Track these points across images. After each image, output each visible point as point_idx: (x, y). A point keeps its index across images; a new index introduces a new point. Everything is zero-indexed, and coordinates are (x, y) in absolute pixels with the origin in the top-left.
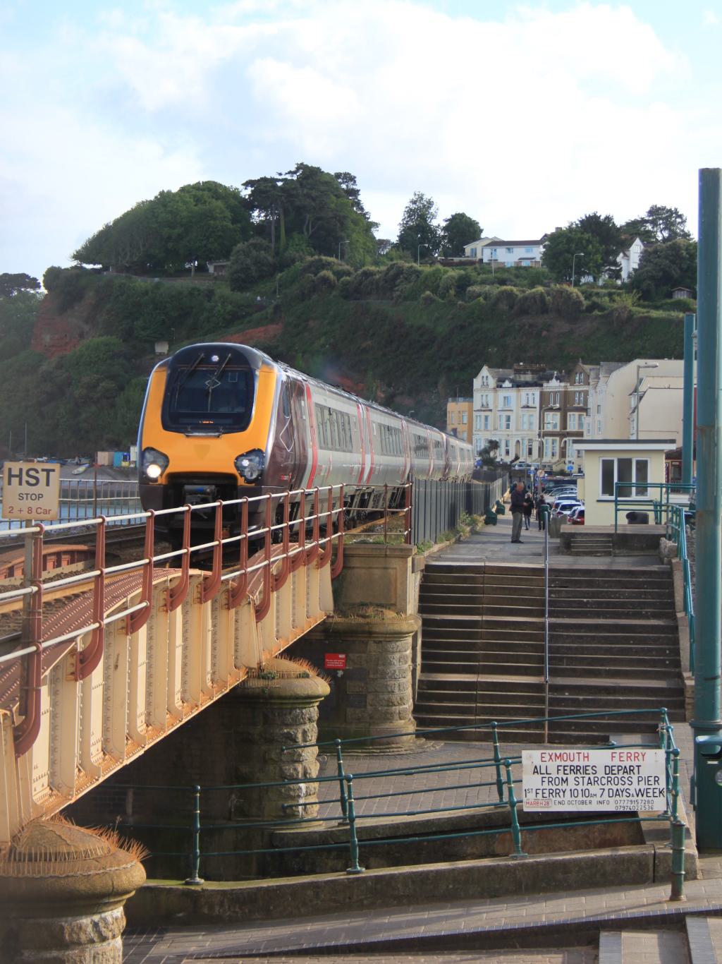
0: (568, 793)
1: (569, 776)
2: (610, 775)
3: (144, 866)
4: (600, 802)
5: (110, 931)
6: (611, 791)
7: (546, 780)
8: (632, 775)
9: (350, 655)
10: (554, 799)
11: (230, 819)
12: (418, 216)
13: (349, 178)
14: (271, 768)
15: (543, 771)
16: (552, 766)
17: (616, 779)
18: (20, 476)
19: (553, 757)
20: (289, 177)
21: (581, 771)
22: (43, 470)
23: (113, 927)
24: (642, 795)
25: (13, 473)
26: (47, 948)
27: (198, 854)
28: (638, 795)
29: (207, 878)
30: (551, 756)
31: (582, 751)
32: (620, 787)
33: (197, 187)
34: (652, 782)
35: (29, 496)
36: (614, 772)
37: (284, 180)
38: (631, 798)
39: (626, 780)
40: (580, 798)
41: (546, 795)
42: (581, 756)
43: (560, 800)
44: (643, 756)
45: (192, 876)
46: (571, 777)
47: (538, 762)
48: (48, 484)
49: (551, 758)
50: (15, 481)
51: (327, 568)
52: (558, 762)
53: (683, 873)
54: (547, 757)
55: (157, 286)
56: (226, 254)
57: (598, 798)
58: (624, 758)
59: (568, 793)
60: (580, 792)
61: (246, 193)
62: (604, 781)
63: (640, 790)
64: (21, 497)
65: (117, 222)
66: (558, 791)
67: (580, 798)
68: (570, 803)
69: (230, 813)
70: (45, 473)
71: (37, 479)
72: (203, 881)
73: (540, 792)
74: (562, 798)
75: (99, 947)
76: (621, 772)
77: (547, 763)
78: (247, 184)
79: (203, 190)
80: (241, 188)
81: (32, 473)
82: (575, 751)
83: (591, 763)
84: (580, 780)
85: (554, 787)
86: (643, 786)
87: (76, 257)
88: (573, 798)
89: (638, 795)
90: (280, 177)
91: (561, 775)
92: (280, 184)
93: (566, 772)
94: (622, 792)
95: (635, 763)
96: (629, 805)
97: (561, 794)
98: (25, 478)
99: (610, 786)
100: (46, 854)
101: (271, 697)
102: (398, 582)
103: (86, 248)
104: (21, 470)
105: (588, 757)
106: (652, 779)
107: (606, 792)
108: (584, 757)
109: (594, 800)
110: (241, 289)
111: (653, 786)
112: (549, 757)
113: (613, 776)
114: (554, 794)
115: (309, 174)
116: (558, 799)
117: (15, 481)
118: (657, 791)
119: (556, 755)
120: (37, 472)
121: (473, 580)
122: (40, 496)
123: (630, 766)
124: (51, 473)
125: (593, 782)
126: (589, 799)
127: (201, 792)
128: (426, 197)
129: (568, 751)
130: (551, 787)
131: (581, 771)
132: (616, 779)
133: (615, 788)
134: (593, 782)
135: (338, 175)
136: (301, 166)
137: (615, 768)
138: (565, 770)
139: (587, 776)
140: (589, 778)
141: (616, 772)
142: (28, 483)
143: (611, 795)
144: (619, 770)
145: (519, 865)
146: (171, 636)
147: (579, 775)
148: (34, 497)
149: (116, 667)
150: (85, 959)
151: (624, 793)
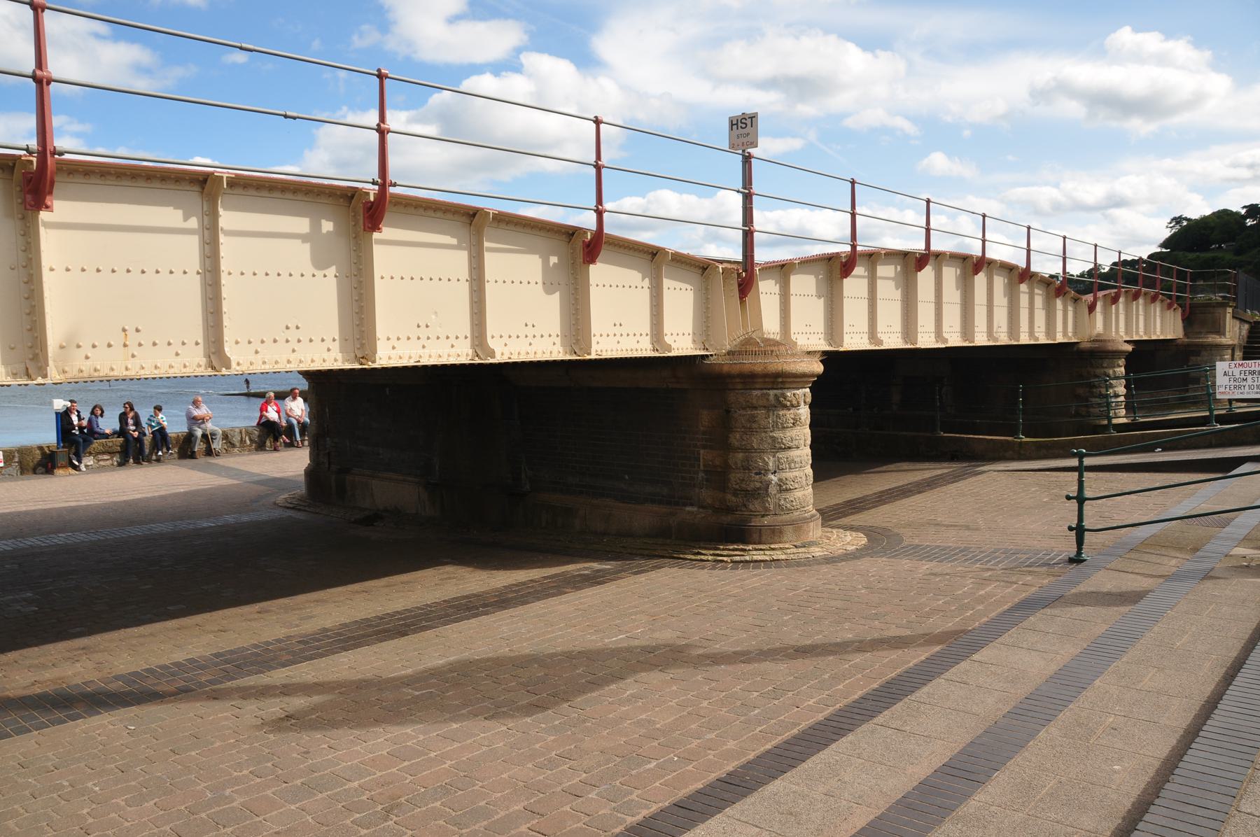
0: (1247, 387)
1: (1248, 377)
16: (1237, 371)
18: (737, 124)
19: (1237, 366)
22: (749, 118)
25: (733, 123)
41: (1232, 388)
46: (1250, 377)
47: (1227, 369)
50: (735, 127)
52: (1241, 368)
54: (1233, 366)
55: (1198, 257)
59: (1247, 387)
60: (1255, 386)
61: (1243, 212)
67: (1255, 390)
68: (1248, 393)
71: (746, 124)
82: (1253, 361)
85: (1238, 384)
91: (1242, 376)
97: (1242, 387)
98: (740, 124)
103: (1164, 242)
104: (737, 120)
116: (1240, 391)
117: (735, 127)
120: (746, 120)
122: (748, 134)
129: (1247, 362)
130: (1235, 383)
142: (741, 127)
146: (1176, 395)
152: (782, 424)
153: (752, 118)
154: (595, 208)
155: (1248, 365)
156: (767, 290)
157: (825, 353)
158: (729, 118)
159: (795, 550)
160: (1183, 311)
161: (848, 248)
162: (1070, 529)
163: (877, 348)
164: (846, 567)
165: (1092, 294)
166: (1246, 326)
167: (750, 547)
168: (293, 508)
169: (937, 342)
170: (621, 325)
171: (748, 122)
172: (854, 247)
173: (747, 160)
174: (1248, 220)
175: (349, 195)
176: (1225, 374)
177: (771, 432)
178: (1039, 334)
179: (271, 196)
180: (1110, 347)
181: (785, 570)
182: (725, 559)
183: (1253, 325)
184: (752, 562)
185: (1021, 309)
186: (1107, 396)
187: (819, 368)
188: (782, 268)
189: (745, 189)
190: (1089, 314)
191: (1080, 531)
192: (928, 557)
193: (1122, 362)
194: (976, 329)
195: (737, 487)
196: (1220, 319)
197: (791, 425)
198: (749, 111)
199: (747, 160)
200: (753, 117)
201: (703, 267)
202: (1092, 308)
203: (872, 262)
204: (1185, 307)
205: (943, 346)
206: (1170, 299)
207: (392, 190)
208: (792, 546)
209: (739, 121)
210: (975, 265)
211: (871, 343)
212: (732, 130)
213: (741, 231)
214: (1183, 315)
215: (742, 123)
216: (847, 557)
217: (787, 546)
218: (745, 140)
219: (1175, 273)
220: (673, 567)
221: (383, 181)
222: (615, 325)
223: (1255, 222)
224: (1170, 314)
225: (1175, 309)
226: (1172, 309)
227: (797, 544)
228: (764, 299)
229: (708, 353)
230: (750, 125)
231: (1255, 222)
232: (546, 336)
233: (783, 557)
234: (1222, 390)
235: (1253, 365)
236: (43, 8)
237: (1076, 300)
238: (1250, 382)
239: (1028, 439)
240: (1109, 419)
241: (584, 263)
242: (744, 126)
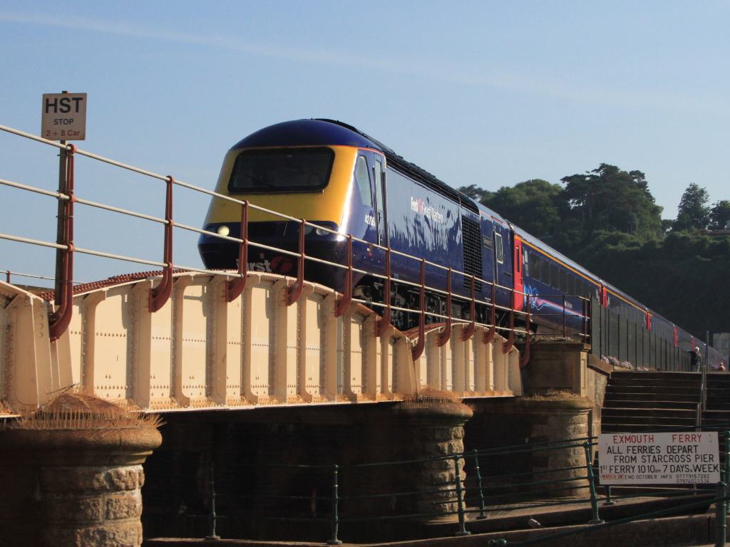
0: (636, 469)
2: (672, 454)
3: (161, 433)
4: (664, 477)
5: (123, 482)
6: (673, 467)
7: (618, 458)
8: (690, 453)
10: (626, 474)
12: (693, 197)
13: (639, 174)
15: (616, 451)
16: (623, 447)
17: (677, 457)
18: (55, 105)
19: (624, 439)
20: (594, 174)
21: (648, 450)
22: (74, 99)
23: (126, 479)
24: (700, 471)
25: (53, 108)
27: (337, 520)
28: (695, 471)
30: (622, 438)
31: (648, 434)
32: (680, 463)
33: (528, 183)
34: (707, 459)
35: (62, 121)
36: (675, 451)
37: (592, 176)
38: (689, 473)
39: (685, 458)
40: (647, 473)
41: (619, 471)
42: (647, 438)
43: (630, 475)
44: (699, 437)
46: (639, 456)
47: (611, 444)
48: (77, 111)
49: (622, 440)
50: (51, 109)
52: (628, 443)
53: (725, 526)
54: (618, 439)
57: (662, 473)
58: (684, 439)
59: (636, 469)
61: (564, 185)
62: (667, 459)
63: (697, 466)
64: (56, 122)
66: (628, 468)
67: (647, 473)
68: (638, 477)
70: (75, 102)
72: (341, 542)
74: (632, 474)
75: (114, 496)
76: (681, 451)
77: (619, 444)
78: (565, 179)
79: (532, 185)
81: (65, 102)
82: (643, 434)
83: (655, 444)
84: (647, 458)
85: (625, 464)
86: (699, 462)
88: (641, 474)
89: (695, 471)
90: (589, 174)
91: (630, 454)
92: (588, 179)
93: (635, 452)
94: (682, 467)
95: (692, 444)
96: (688, 478)
97: (631, 470)
98: (59, 106)
99: (671, 463)
100: (73, 414)
105: (652, 439)
106: (707, 457)
107: (669, 467)
108: (650, 439)
109: (659, 474)
111: (708, 463)
112: (620, 440)
113: (674, 455)
114: (625, 470)
115: (609, 171)
117: (51, 109)
118: (712, 467)
119: (626, 437)
120: (68, 100)
122: (71, 121)
123: (689, 446)
124: (80, 102)
125: (657, 459)
127: (339, 470)
128: (700, 187)
129: (635, 434)
130: (622, 464)
131: (648, 450)
132: (677, 457)
133: (676, 464)
134: (657, 459)
135: (632, 173)
136: (603, 166)
137: (676, 448)
138: (633, 450)
139: (652, 455)
140: (654, 457)
141: (676, 451)
142: (61, 110)
143: (673, 470)
144: (679, 450)
147: (645, 454)
148: (66, 122)
150: (99, 503)
151: (684, 469)
152: (115, 513)
157: (165, 417)
158: (44, 95)
160: (522, 355)
163: (183, 409)
166: (603, 379)
169: (209, 402)
170: (110, 377)
171: (73, 104)
173: (67, 155)
174: (571, 201)
177: (100, 524)
178: (191, 390)
180: (446, 409)
185: (228, 346)
187: (155, 438)
190: (52, 340)
193: (459, 430)
194: (152, 382)
197: (125, 514)
199: (67, 155)
200: (80, 99)
205: (252, 407)
206: (381, 314)
209: (58, 102)
211: (209, 402)
212: (47, 111)
218: (66, 128)
221: (168, 271)
222: (106, 377)
224: (504, 359)
226: (508, 353)
234: (606, 472)
235: (643, 438)
237: (395, 341)
238: (639, 462)
242: (65, 109)
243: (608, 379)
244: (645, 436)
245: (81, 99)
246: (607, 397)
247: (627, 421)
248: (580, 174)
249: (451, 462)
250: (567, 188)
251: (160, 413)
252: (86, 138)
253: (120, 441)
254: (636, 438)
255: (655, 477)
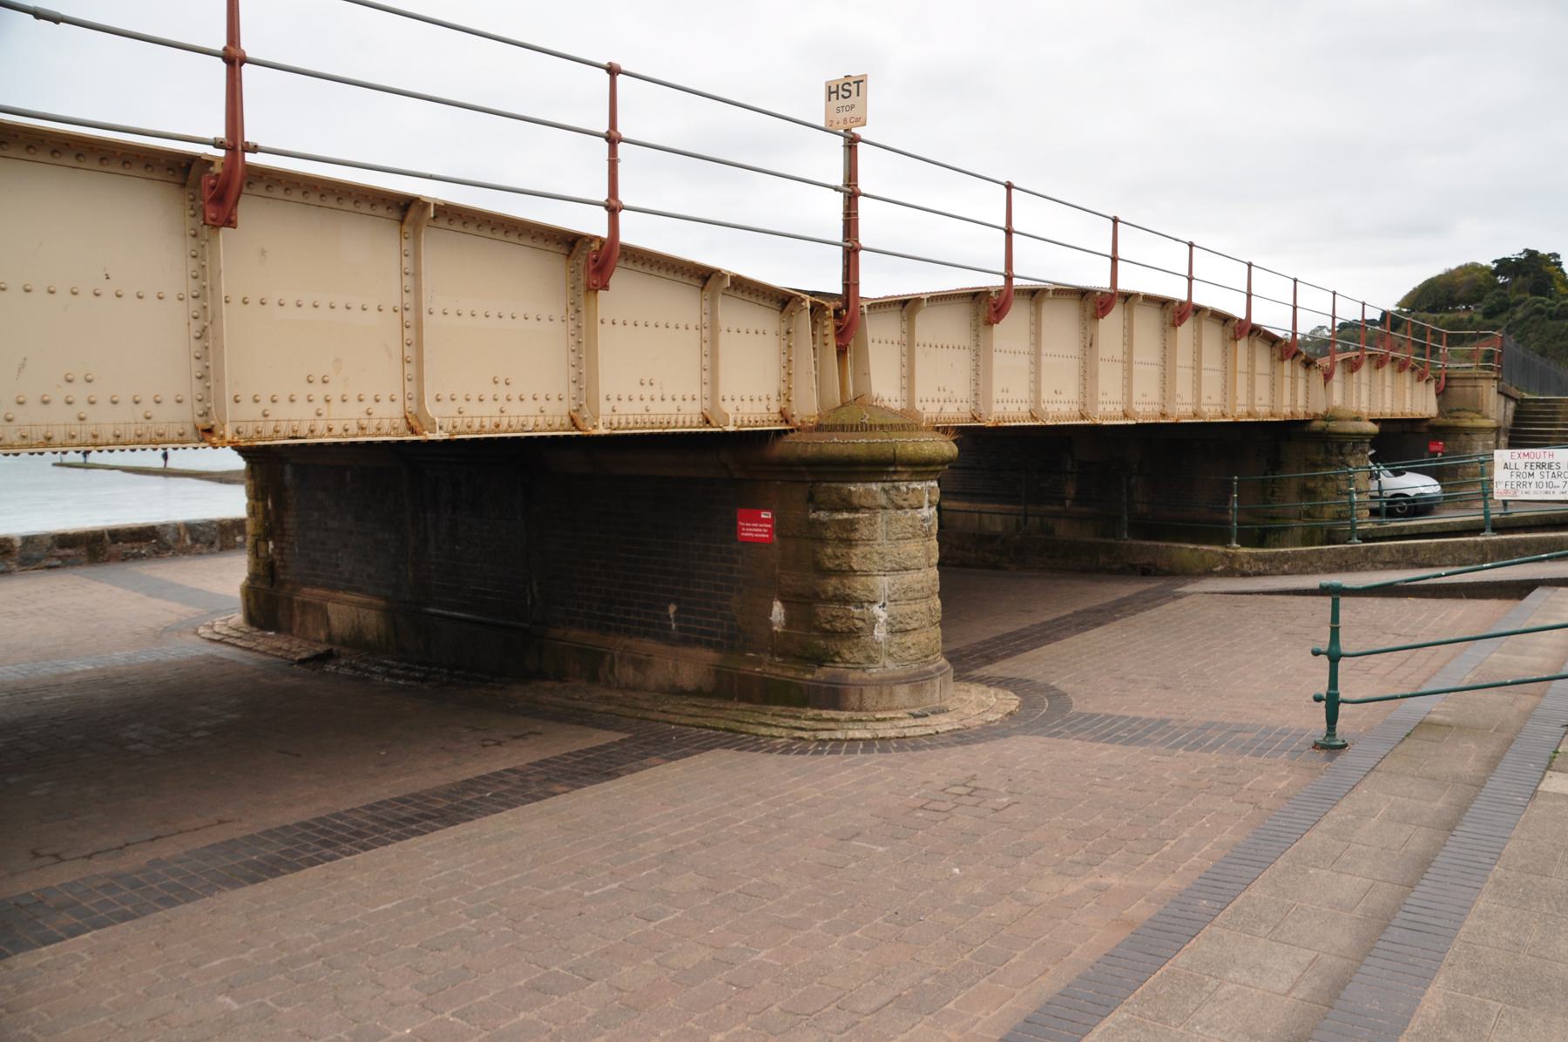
0: (1533, 485)
7: (1514, 474)
9: (1448, 443)
11: (1300, 519)
13: (1556, 256)
14: (1330, 484)
15: (1513, 467)
16: (1521, 465)
18: (837, 92)
19: (1521, 456)
20: (1519, 256)
21: (1547, 467)
22: (854, 82)
25: (832, 90)
26: (839, 510)
29: (1244, 545)
37: (1516, 258)
40: (1545, 489)
42: (1547, 455)
43: (1526, 490)
45: (1230, 542)
46: (1537, 472)
47: (1508, 460)
48: (858, 95)
51: (1432, 386)
52: (1526, 459)
56: (1479, 300)
57: (1561, 489)
59: (1533, 485)
60: (1545, 484)
61: (1495, 265)
65: (1420, 286)
67: (1545, 489)
68: (1535, 493)
69: (1300, 514)
70: (856, 85)
71: (850, 91)
73: (1509, 484)
74: (1528, 489)
77: (1516, 461)
78: (1494, 262)
80: (1491, 264)
81: (847, 94)
83: (1555, 460)
84: (1545, 475)
85: (1522, 480)
87: (1397, 305)
91: (1528, 470)
92: (1513, 260)
98: (841, 92)
101: (1330, 433)
102: (1485, 395)
104: (838, 86)
109: (1557, 490)
110: (1489, 318)
115: (1532, 255)
120: (850, 85)
121: (1554, 407)
122: (852, 107)
124: (861, 84)
126: (1553, 489)
127: (1238, 481)
130: (1518, 479)
131: (1547, 467)
135: (1550, 255)
136: (1526, 250)
142: (843, 96)
145: (1487, 541)
149: (1091, 345)
153: (858, 82)
154: (607, 203)
155: (1535, 455)
156: (880, 339)
158: (827, 83)
159: (912, 722)
161: (1000, 281)
162: (1318, 699)
164: (983, 753)
165: (1328, 357)
166: (1512, 405)
167: (844, 715)
168: (219, 641)
171: (854, 88)
172: (1009, 278)
174: (1499, 277)
175: (184, 165)
176: (1506, 466)
179: (106, 169)
181: (894, 757)
182: (805, 735)
183: (1519, 402)
184: (846, 740)
186: (1350, 494)
188: (903, 306)
189: (849, 186)
191: (1332, 703)
192: (1108, 735)
195: (828, 627)
196: (1482, 395)
198: (855, 73)
199: (852, 143)
201: (783, 300)
202: (1328, 377)
203: (1036, 304)
204: (1440, 378)
207: (250, 158)
208: (907, 716)
210: (1176, 312)
212: (830, 100)
213: (841, 248)
214: (1437, 388)
215: (844, 90)
216: (987, 733)
217: (899, 715)
219: (1429, 333)
220: (728, 748)
221: (234, 142)
223: (1507, 280)
225: (1427, 381)
227: (916, 711)
228: (874, 351)
229: (787, 428)
230: (856, 94)
231: (1507, 280)
232: (528, 398)
233: (892, 733)
236: (244, 60)
239: (1245, 550)
240: (1353, 525)
241: (588, 289)
242: (847, 94)
243: (1517, 404)
244: (1545, 452)
245: (862, 81)
246: (1515, 418)
247: (1530, 439)
248: (1507, 257)
249: (1231, 512)
250: (1496, 268)
251: (958, 427)
252: (867, 123)
253: (895, 454)
254: (1535, 455)
255: (1554, 492)
